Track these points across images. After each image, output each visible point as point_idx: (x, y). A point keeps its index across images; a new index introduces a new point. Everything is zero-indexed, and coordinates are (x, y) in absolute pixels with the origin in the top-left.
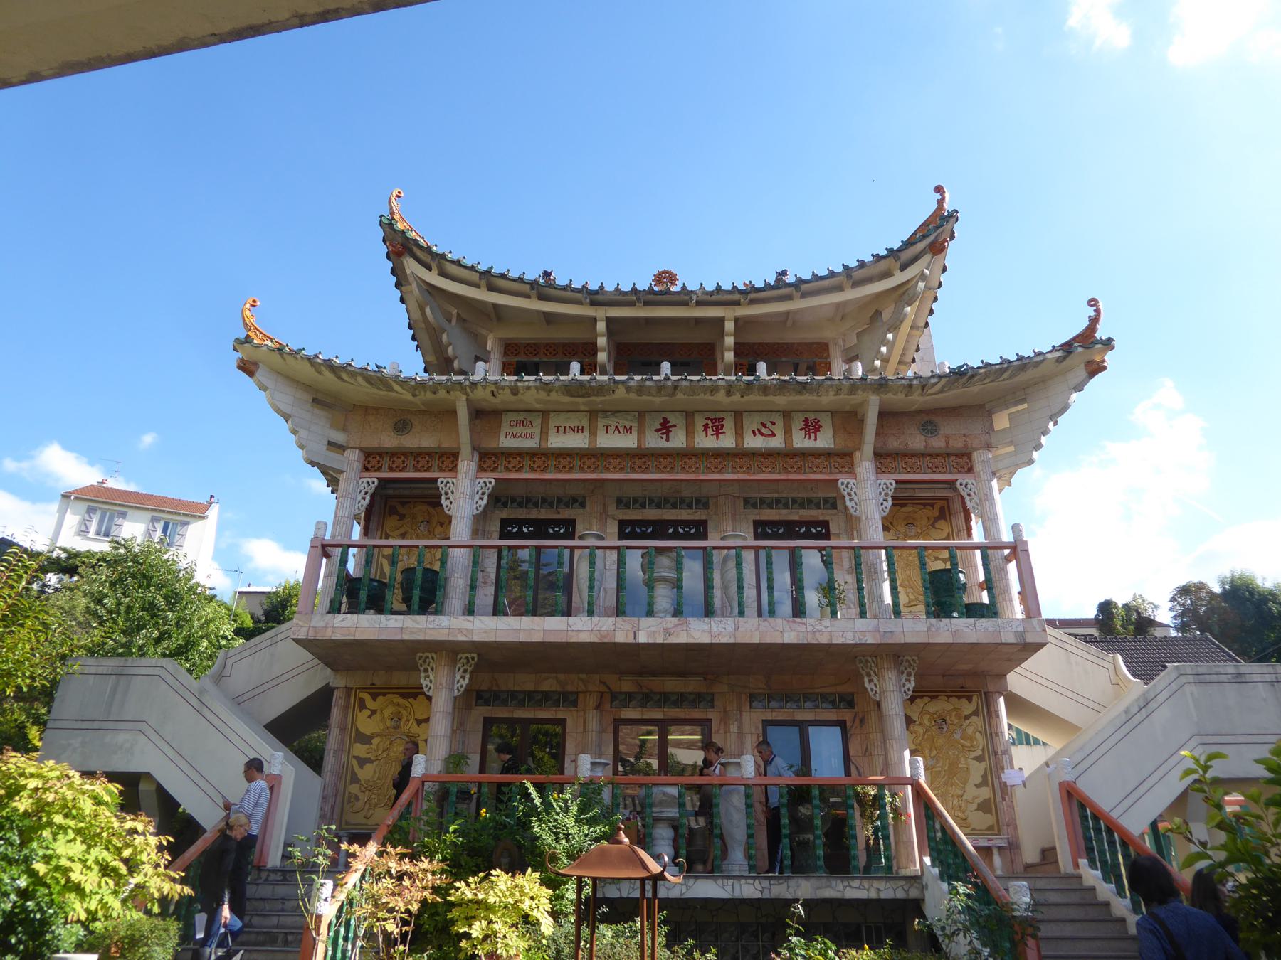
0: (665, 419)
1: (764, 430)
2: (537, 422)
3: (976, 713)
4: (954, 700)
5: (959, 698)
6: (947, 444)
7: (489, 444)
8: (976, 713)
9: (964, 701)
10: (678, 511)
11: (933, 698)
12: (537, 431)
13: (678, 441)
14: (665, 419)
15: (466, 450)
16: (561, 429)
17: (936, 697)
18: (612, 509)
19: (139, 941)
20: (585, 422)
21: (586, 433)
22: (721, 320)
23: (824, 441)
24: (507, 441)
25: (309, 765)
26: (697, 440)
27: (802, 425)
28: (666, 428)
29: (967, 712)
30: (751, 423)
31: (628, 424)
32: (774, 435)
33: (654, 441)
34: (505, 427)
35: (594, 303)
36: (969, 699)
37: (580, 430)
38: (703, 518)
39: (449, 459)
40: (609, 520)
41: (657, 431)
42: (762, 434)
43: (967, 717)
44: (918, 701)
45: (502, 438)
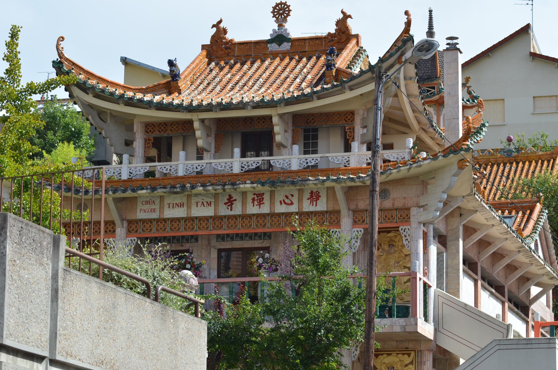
0: (230, 196)
1: (287, 201)
2: (158, 201)
3: (411, 363)
4: (400, 356)
5: (403, 354)
6: (393, 205)
7: (131, 216)
8: (411, 363)
9: (406, 356)
10: (253, 242)
11: (389, 355)
12: (157, 207)
13: (237, 210)
14: (230, 196)
15: (118, 222)
16: (171, 205)
17: (390, 354)
18: (214, 242)
19: (135, 252)
20: (184, 200)
21: (185, 208)
22: (270, 118)
23: (321, 206)
24: (141, 215)
25: (459, 291)
26: (248, 209)
27: (308, 196)
28: (230, 202)
29: (407, 362)
30: (279, 197)
31: (209, 200)
32: (292, 203)
33: (224, 211)
34: (140, 206)
35: (190, 111)
36: (409, 355)
37: (182, 205)
38: (268, 245)
39: (332, 217)
40: (212, 249)
41: (225, 204)
42: (285, 203)
43: (406, 366)
44: (380, 356)
45: (138, 213)
